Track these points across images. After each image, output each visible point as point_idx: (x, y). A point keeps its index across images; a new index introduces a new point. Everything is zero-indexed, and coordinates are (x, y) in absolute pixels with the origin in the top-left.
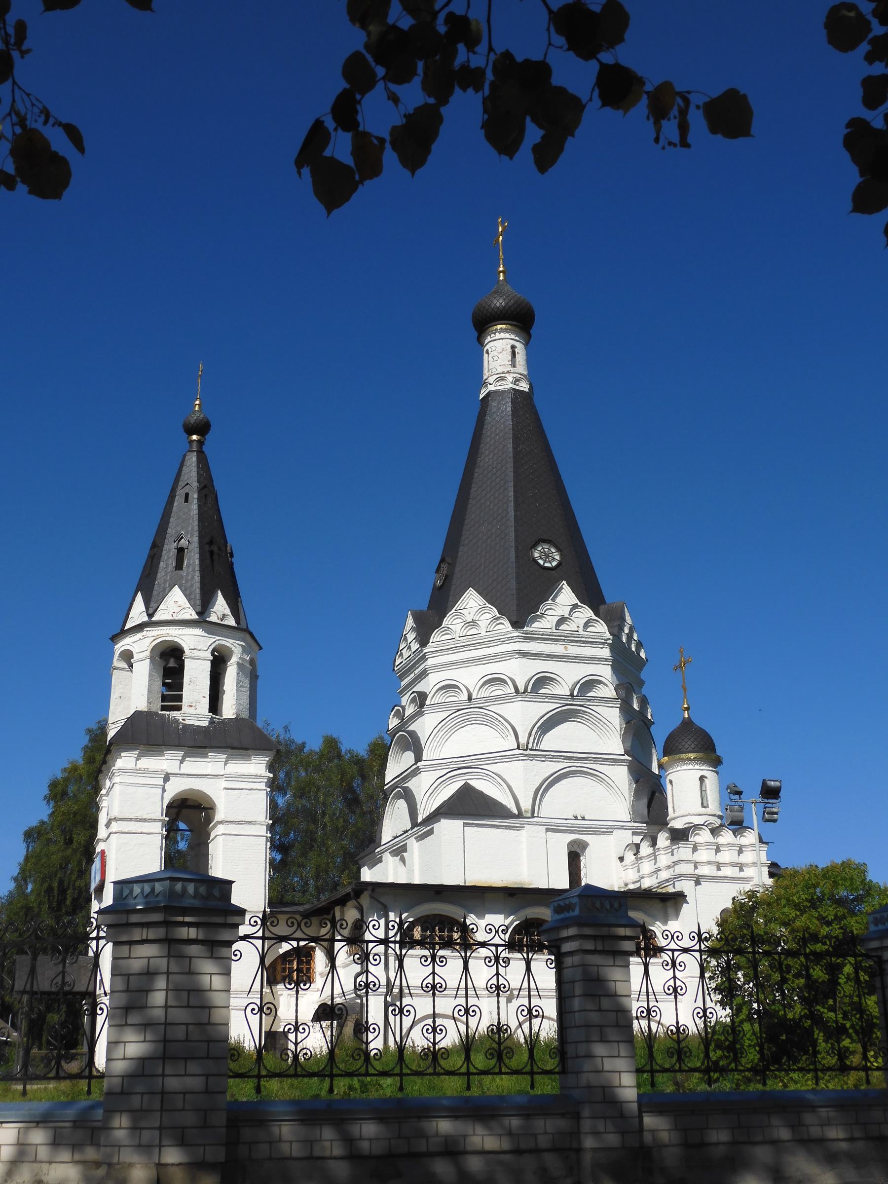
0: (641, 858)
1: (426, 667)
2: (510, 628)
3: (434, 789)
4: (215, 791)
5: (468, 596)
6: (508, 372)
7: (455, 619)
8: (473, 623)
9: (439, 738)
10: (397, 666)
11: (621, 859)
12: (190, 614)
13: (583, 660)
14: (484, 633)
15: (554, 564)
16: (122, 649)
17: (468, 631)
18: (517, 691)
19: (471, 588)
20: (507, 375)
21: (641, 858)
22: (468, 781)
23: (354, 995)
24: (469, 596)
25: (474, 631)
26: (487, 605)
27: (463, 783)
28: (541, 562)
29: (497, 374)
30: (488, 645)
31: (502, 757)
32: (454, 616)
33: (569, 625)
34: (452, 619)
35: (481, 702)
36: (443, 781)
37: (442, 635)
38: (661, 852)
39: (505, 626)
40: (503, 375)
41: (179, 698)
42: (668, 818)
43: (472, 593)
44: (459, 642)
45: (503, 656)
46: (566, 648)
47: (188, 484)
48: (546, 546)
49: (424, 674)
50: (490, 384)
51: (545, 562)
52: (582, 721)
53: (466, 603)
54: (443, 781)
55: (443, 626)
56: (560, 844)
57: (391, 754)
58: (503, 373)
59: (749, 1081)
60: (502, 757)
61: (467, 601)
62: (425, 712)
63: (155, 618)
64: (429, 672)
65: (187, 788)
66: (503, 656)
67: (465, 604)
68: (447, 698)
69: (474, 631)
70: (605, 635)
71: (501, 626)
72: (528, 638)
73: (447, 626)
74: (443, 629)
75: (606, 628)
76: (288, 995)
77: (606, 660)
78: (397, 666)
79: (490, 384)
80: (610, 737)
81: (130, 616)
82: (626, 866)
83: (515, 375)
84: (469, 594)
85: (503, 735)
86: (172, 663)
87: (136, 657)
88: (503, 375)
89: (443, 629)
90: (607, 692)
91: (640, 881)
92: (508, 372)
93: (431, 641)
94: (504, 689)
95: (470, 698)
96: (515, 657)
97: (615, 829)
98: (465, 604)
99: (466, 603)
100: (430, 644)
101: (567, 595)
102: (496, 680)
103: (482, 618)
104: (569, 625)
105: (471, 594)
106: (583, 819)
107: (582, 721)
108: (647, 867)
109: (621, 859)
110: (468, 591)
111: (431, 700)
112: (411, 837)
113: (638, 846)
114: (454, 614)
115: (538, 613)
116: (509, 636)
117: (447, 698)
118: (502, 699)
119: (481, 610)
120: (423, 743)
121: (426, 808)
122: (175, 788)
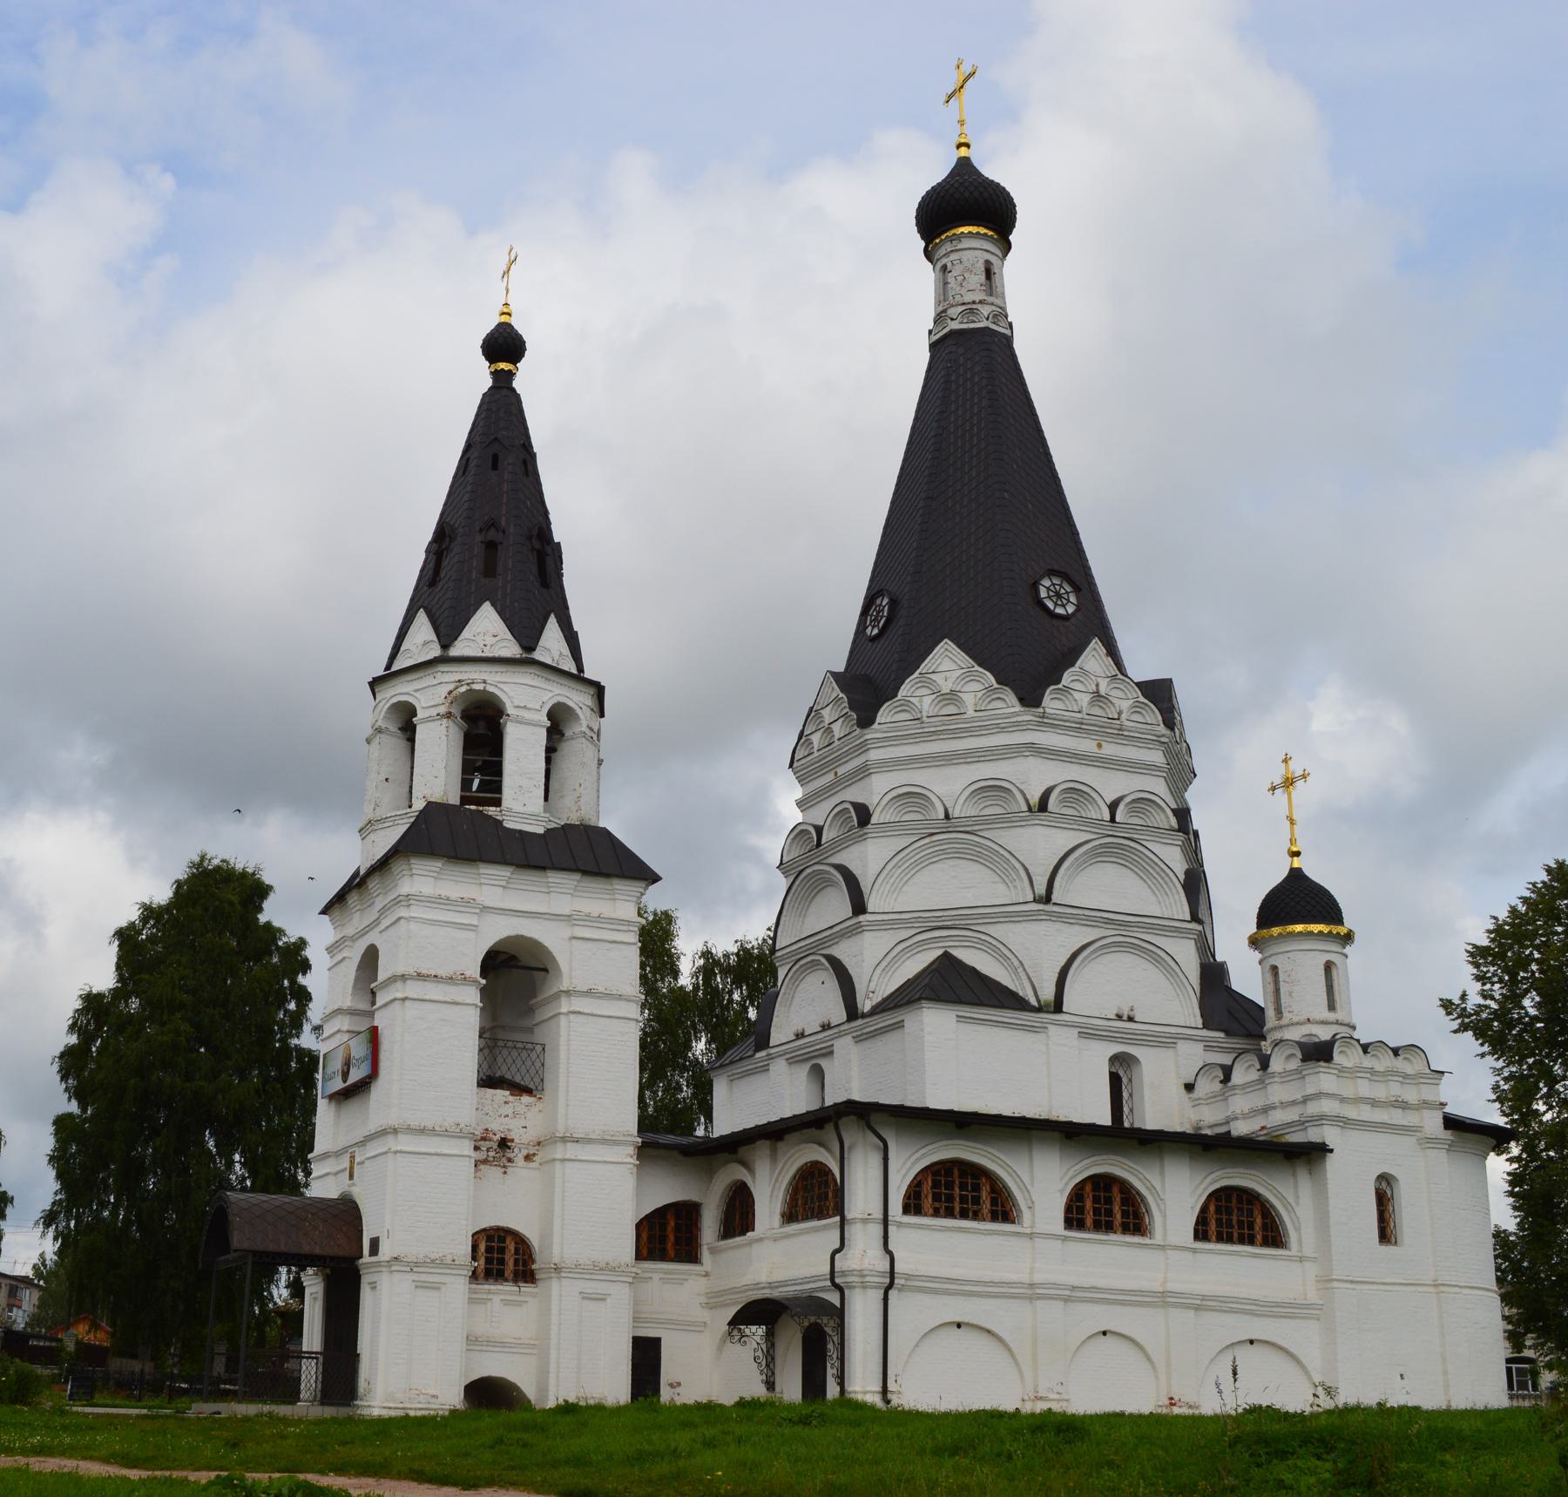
0: (1234, 1088)
1: (868, 763)
2: (1018, 708)
3: (890, 960)
4: (550, 937)
5: (940, 652)
6: (980, 302)
7: (917, 688)
8: (953, 697)
9: (893, 879)
10: (798, 761)
11: (1189, 1087)
12: (511, 649)
13: (1125, 766)
14: (971, 713)
15: (1060, 611)
16: (395, 700)
17: (942, 707)
18: (1030, 810)
19: (946, 640)
20: (979, 306)
21: (1234, 1088)
22: (948, 950)
23: (829, 1283)
24: (944, 652)
25: (952, 709)
26: (977, 668)
27: (940, 952)
28: (1050, 605)
29: (964, 304)
30: (976, 734)
31: (1007, 914)
32: (916, 683)
33: (1104, 709)
34: (913, 689)
35: (968, 823)
36: (906, 949)
37: (896, 713)
38: (1276, 1079)
39: (1009, 703)
40: (974, 306)
41: (499, 790)
42: (1265, 1029)
43: (949, 648)
44: (926, 725)
45: (1004, 751)
46: (1099, 746)
47: (496, 439)
48: (1056, 581)
49: (863, 772)
50: (952, 319)
51: (1056, 604)
52: (1127, 864)
53: (938, 662)
54: (906, 949)
55: (899, 697)
56: (1098, 1057)
57: (791, 900)
58: (974, 302)
59: (813, 1411)
60: (1007, 914)
61: (939, 660)
62: (870, 835)
63: (454, 652)
64: (871, 771)
65: (512, 933)
66: (1004, 751)
67: (935, 666)
68: (981, 809)
69: (952, 709)
70: (1158, 728)
71: (999, 704)
72: (1046, 723)
73: (906, 698)
74: (898, 703)
75: (1160, 718)
76: (660, 1279)
77: (1158, 768)
78: (798, 761)
79: (952, 319)
80: (1169, 892)
81: (402, 649)
82: (1199, 1099)
83: (994, 308)
84: (943, 650)
85: (1006, 879)
86: (481, 729)
87: (421, 714)
88: (974, 306)
89: (898, 703)
90: (1161, 820)
91: (1228, 1122)
92: (980, 302)
93: (878, 720)
94: (1003, 804)
95: (947, 816)
96: (1025, 754)
97: (1180, 1038)
98: (935, 666)
99: (938, 662)
100: (875, 726)
101: (1100, 661)
102: (992, 790)
103: (965, 689)
104: (1104, 709)
105: (946, 649)
106: (1131, 1019)
107: (1127, 864)
108: (1240, 1103)
109: (1189, 1087)
110: (942, 644)
111: (879, 817)
112: (847, 1034)
113: (1227, 1072)
114: (918, 680)
115: (1060, 686)
116: (1014, 720)
117: (981, 809)
118: (1007, 820)
119: (964, 676)
120: (866, 890)
121: (875, 986)
122: (495, 931)
